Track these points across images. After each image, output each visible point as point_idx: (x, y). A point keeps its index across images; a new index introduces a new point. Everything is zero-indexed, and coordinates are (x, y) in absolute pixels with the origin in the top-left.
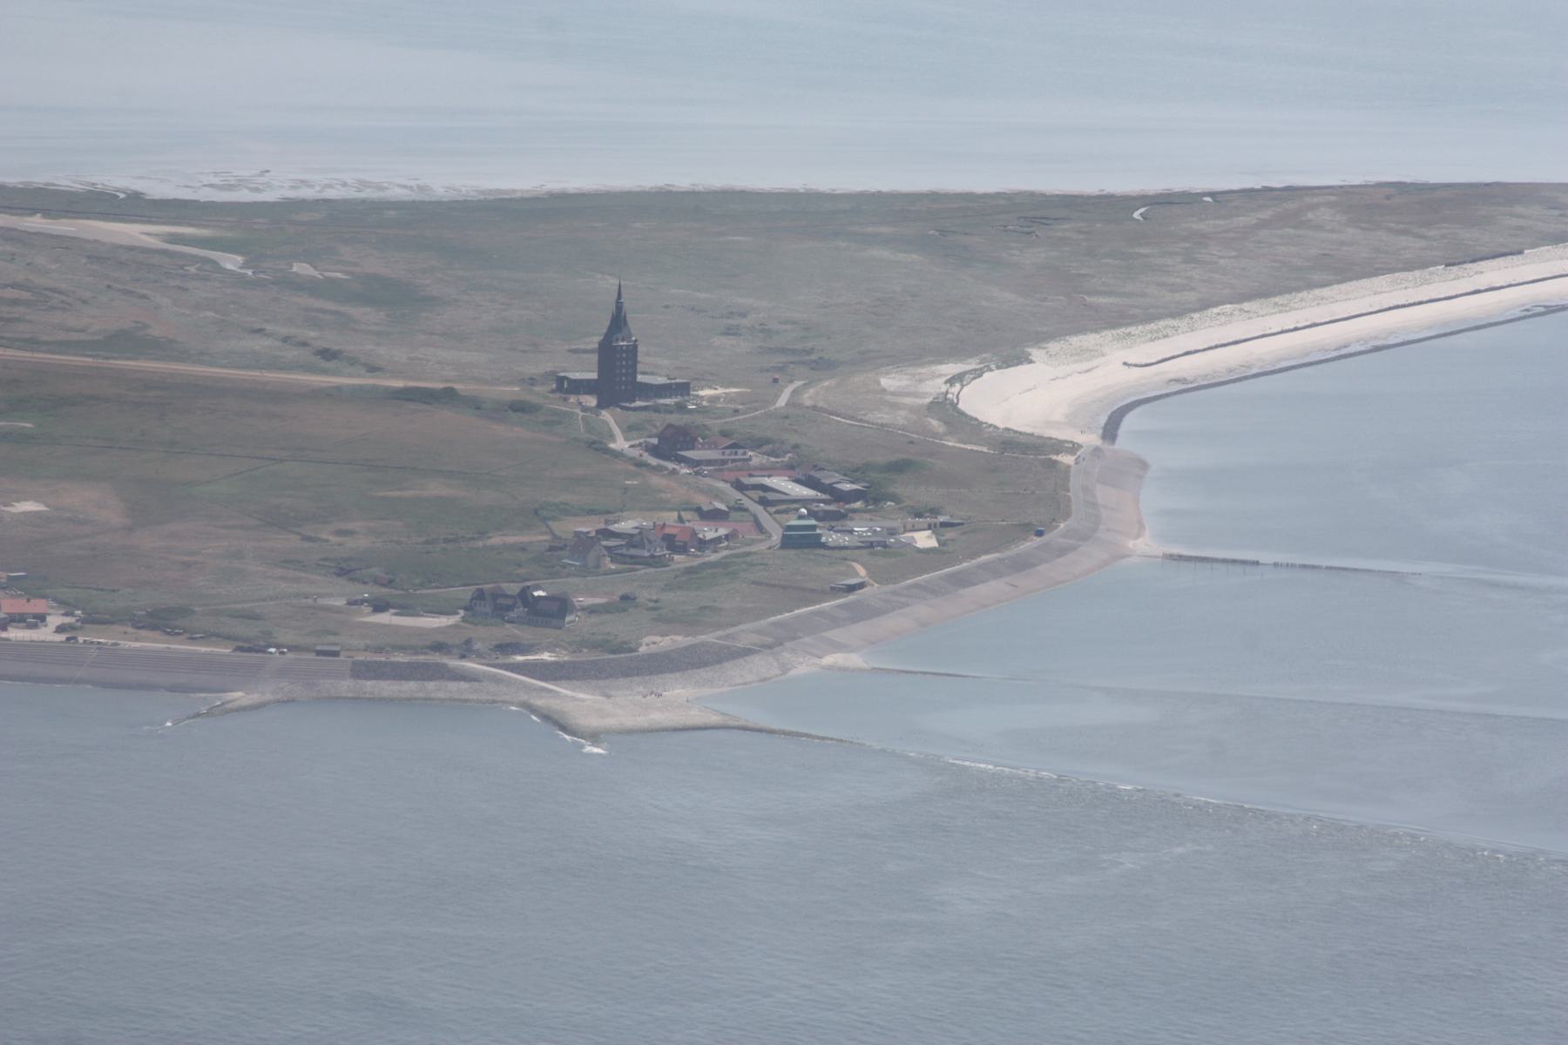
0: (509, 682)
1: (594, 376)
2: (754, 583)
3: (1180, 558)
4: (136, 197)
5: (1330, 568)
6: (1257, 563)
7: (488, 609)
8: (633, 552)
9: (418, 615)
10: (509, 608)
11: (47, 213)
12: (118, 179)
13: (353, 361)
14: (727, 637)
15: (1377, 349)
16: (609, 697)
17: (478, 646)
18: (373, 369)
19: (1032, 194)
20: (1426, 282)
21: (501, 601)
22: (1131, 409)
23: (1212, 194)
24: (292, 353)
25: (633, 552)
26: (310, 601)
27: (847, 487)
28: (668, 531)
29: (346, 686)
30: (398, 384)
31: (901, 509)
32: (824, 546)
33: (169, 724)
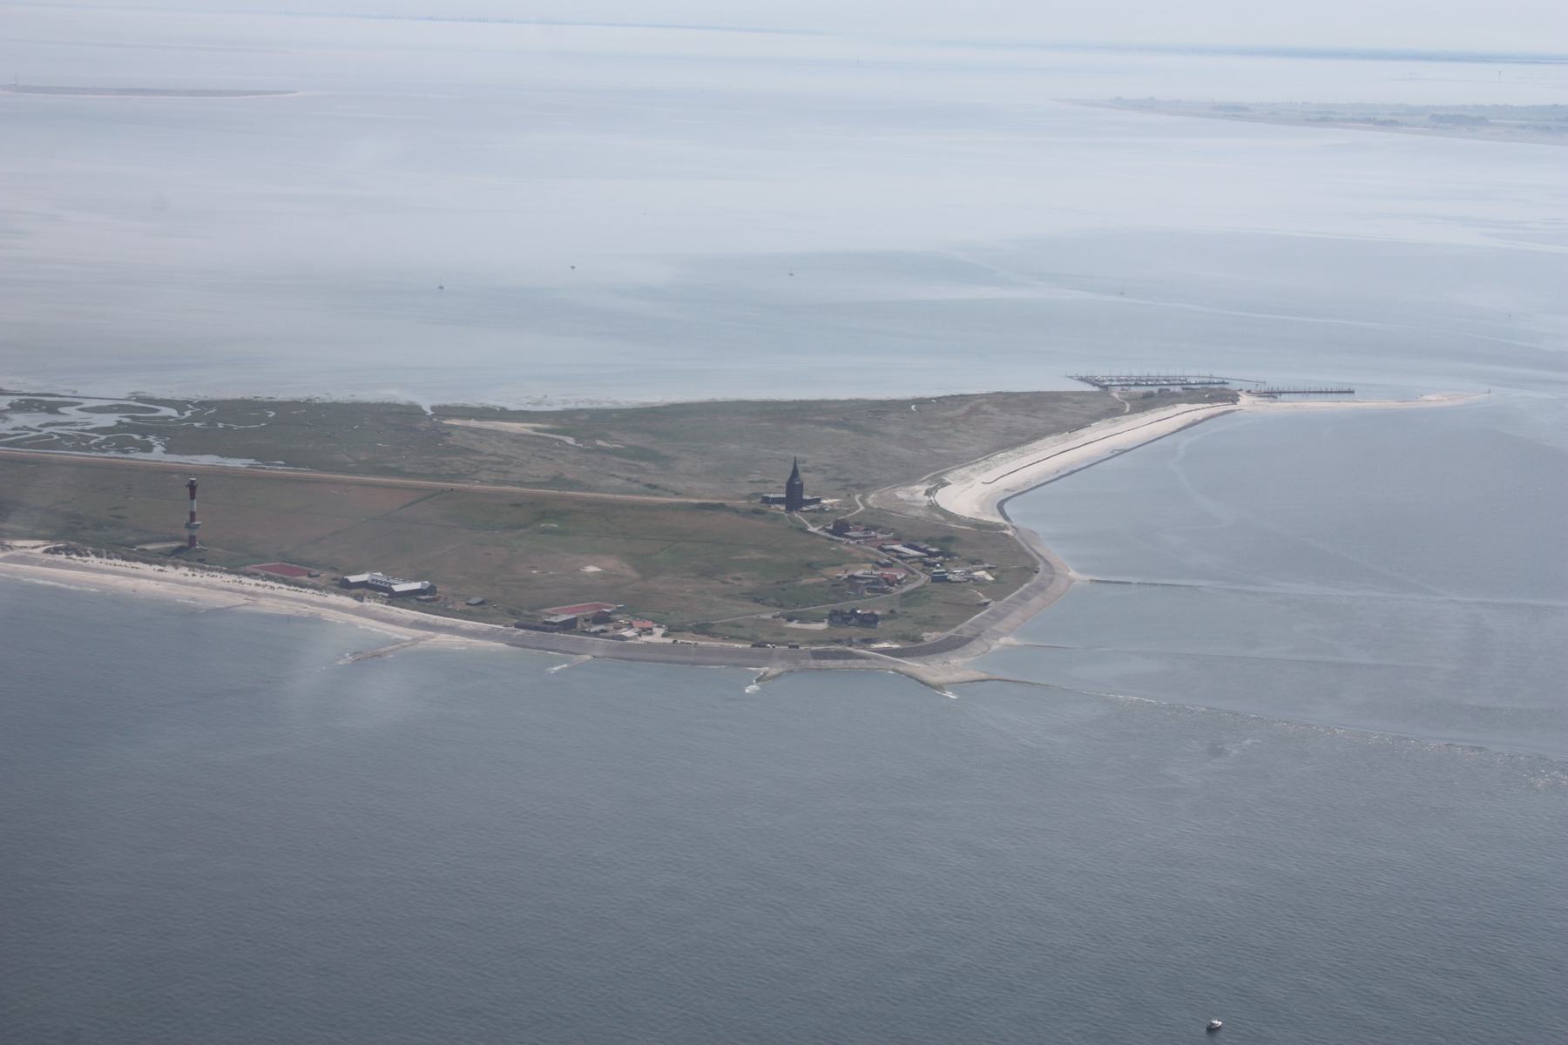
0: (883, 659)
1: (784, 496)
2: (944, 602)
3: (1098, 581)
4: (503, 410)
5: (1163, 585)
6: (1130, 583)
7: (840, 620)
8: (875, 587)
9: (809, 623)
10: (850, 619)
11: (476, 418)
12: (492, 400)
13: (665, 490)
14: (958, 632)
15: (1072, 473)
16: (929, 665)
17: (854, 640)
18: (677, 494)
19: (857, 401)
20: (1066, 441)
21: (845, 616)
22: (92, 408)
23: (935, 399)
24: (635, 486)
25: (875, 587)
26: (755, 616)
27: (934, 550)
28: (885, 576)
29: (812, 663)
30: (696, 501)
31: (1054, 573)
32: (950, 581)
33: (220, 425)
